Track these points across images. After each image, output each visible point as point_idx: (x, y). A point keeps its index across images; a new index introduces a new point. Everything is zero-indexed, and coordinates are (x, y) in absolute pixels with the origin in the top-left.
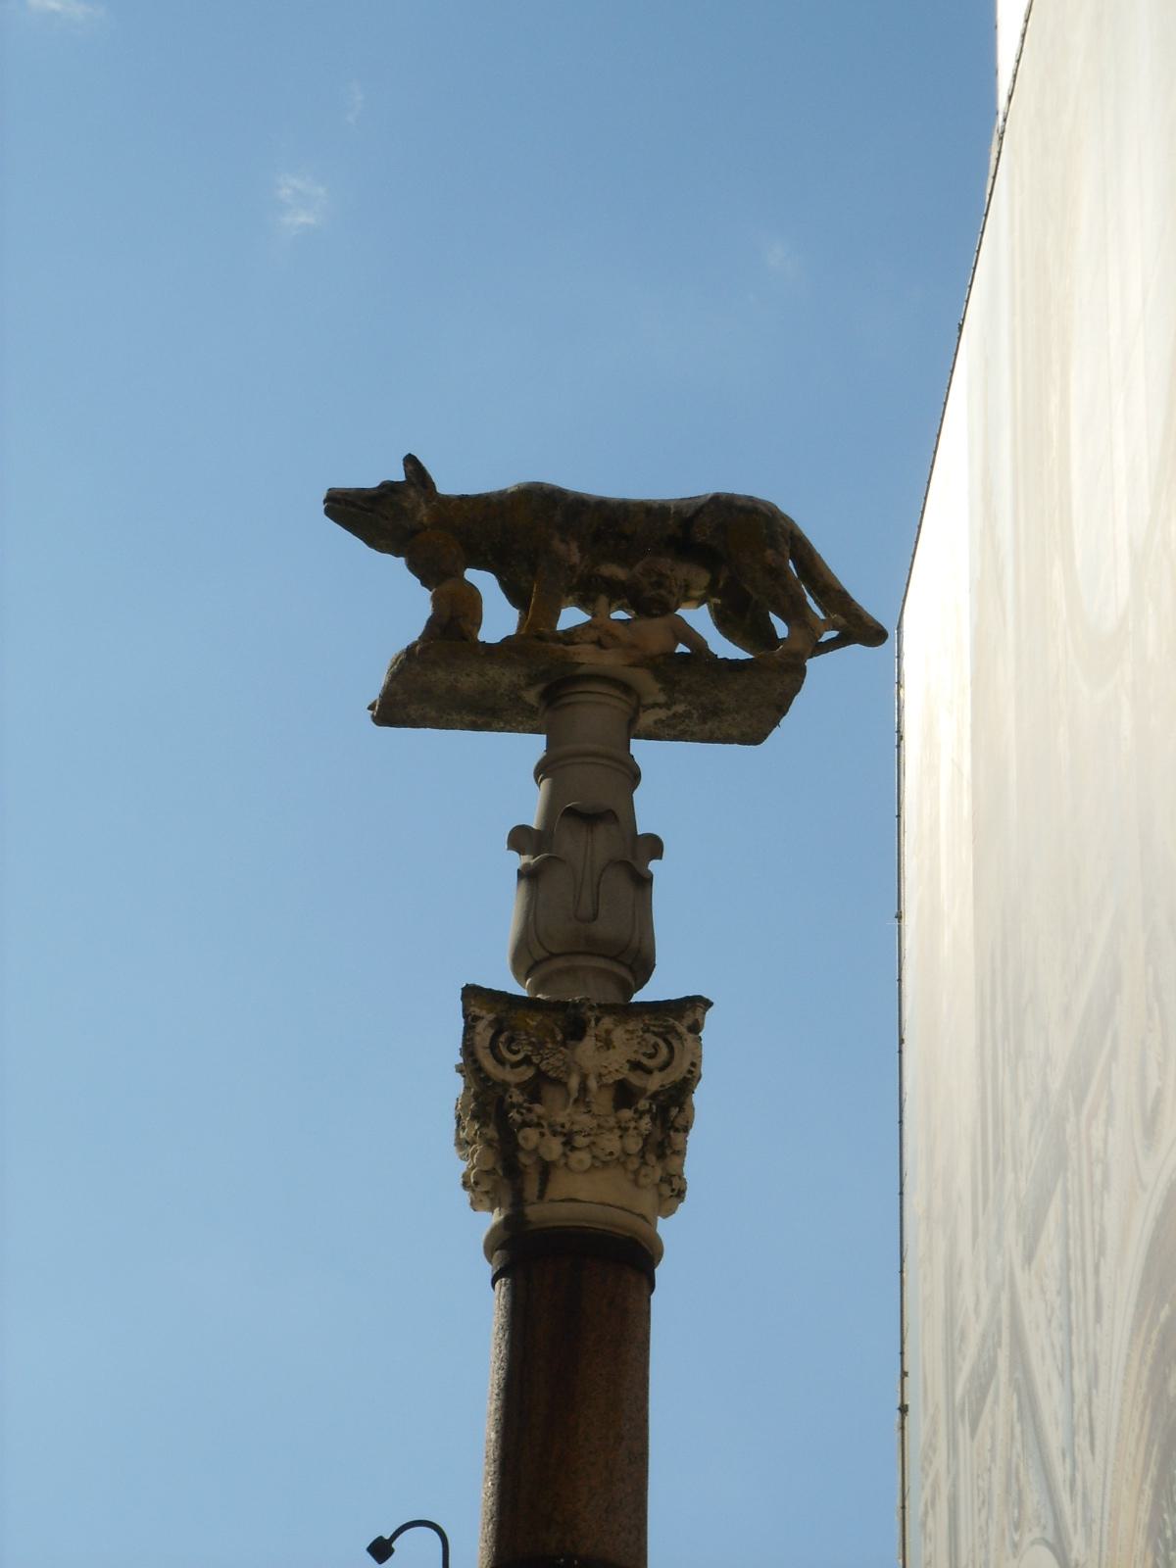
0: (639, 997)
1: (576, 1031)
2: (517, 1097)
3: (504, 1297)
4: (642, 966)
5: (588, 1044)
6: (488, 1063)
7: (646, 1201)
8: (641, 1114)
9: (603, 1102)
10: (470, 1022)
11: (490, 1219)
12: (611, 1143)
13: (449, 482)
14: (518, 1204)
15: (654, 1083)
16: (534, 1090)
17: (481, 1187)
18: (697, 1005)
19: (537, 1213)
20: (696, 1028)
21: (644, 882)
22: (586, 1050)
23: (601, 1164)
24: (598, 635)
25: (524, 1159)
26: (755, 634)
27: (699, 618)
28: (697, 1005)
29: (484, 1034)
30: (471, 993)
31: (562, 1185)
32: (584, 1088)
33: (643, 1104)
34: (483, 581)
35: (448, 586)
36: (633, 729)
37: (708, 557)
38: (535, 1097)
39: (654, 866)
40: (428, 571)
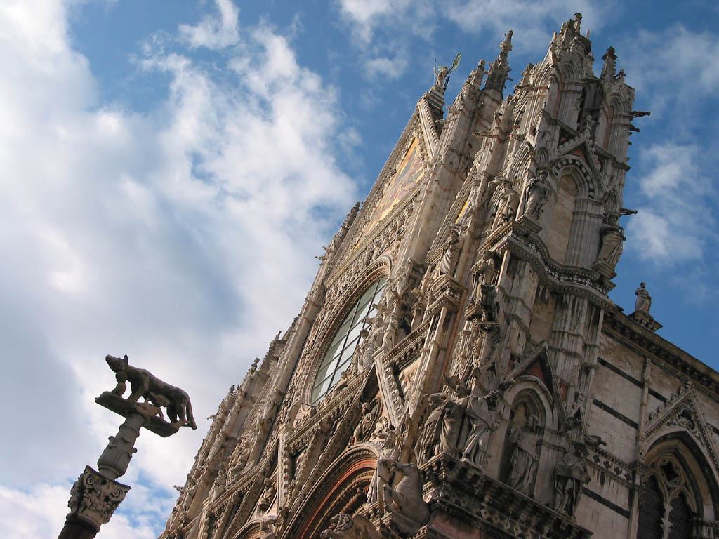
0: (116, 480)
1: (104, 483)
2: (87, 491)
3: (296, 348)
4: (122, 473)
5: (105, 486)
6: (85, 483)
7: (102, 520)
8: (108, 504)
9: (102, 498)
10: (85, 472)
11: (69, 511)
12: (100, 507)
13: (131, 363)
14: (78, 510)
15: (113, 499)
16: (91, 490)
17: (71, 504)
18: (615, 286)
19: (80, 514)
20: (126, 492)
21: (130, 457)
22: (104, 487)
23: (96, 510)
24: (143, 406)
25: (82, 503)
26: (173, 419)
27: (164, 410)
28: (615, 286)
29: (87, 476)
30: (88, 467)
31: (87, 511)
32: (100, 494)
33: (109, 502)
34: (128, 384)
35: (121, 384)
36: (143, 425)
37: (170, 399)
38: (90, 493)
39: (133, 455)
40: (120, 379)
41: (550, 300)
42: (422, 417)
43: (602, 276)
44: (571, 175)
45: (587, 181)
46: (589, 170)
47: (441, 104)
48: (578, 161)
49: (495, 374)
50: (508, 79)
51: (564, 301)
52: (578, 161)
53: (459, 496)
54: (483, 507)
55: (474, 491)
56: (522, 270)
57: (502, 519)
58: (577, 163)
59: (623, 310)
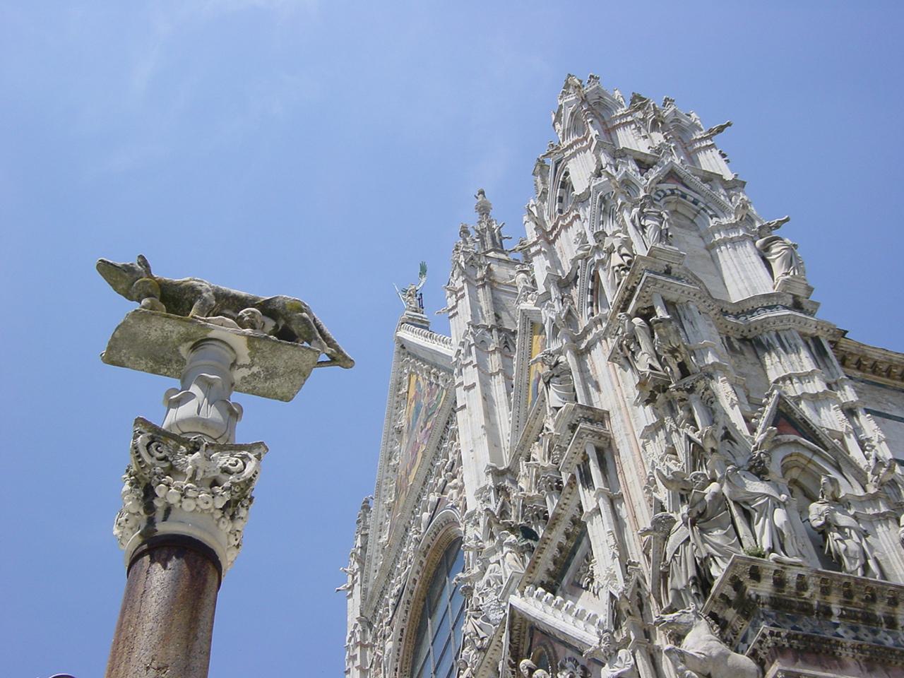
18: (818, 304)
28: (818, 304)
41: (743, 348)
42: (639, 594)
43: (795, 297)
44: (676, 211)
45: (703, 209)
46: (697, 196)
47: (426, 325)
48: (676, 189)
49: (735, 441)
50: (504, 238)
51: (765, 343)
52: (676, 189)
53: (793, 619)
54: (836, 625)
55: (811, 606)
56: (687, 313)
57: (875, 632)
58: (676, 192)
59: (846, 332)
